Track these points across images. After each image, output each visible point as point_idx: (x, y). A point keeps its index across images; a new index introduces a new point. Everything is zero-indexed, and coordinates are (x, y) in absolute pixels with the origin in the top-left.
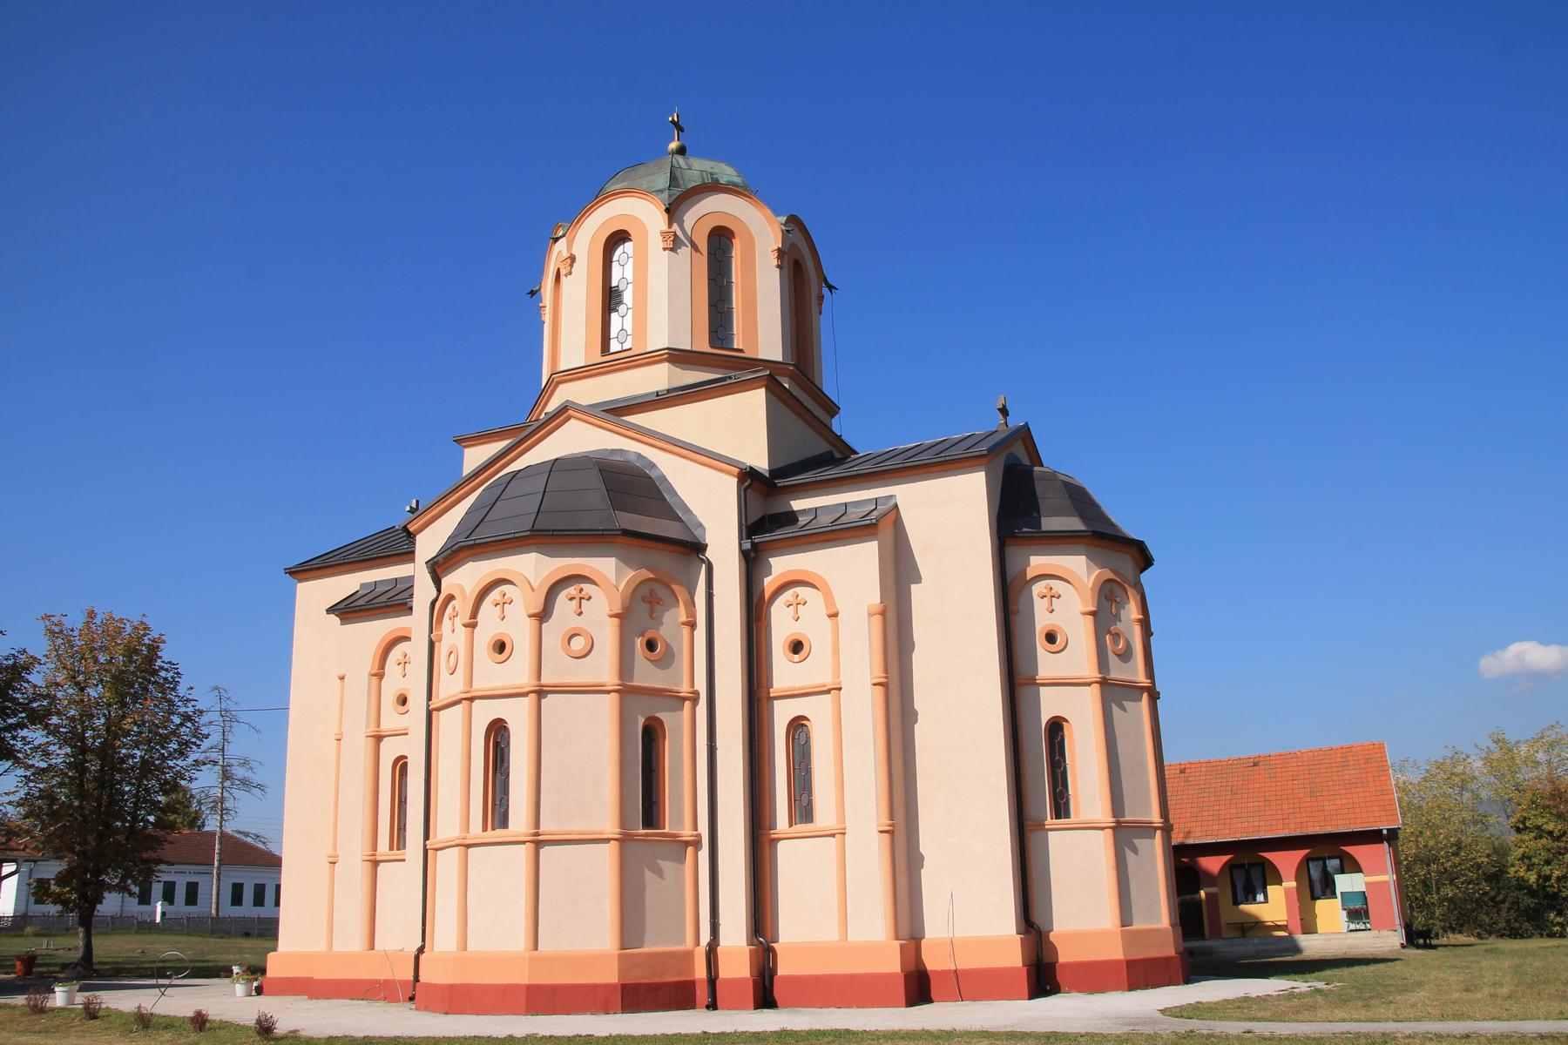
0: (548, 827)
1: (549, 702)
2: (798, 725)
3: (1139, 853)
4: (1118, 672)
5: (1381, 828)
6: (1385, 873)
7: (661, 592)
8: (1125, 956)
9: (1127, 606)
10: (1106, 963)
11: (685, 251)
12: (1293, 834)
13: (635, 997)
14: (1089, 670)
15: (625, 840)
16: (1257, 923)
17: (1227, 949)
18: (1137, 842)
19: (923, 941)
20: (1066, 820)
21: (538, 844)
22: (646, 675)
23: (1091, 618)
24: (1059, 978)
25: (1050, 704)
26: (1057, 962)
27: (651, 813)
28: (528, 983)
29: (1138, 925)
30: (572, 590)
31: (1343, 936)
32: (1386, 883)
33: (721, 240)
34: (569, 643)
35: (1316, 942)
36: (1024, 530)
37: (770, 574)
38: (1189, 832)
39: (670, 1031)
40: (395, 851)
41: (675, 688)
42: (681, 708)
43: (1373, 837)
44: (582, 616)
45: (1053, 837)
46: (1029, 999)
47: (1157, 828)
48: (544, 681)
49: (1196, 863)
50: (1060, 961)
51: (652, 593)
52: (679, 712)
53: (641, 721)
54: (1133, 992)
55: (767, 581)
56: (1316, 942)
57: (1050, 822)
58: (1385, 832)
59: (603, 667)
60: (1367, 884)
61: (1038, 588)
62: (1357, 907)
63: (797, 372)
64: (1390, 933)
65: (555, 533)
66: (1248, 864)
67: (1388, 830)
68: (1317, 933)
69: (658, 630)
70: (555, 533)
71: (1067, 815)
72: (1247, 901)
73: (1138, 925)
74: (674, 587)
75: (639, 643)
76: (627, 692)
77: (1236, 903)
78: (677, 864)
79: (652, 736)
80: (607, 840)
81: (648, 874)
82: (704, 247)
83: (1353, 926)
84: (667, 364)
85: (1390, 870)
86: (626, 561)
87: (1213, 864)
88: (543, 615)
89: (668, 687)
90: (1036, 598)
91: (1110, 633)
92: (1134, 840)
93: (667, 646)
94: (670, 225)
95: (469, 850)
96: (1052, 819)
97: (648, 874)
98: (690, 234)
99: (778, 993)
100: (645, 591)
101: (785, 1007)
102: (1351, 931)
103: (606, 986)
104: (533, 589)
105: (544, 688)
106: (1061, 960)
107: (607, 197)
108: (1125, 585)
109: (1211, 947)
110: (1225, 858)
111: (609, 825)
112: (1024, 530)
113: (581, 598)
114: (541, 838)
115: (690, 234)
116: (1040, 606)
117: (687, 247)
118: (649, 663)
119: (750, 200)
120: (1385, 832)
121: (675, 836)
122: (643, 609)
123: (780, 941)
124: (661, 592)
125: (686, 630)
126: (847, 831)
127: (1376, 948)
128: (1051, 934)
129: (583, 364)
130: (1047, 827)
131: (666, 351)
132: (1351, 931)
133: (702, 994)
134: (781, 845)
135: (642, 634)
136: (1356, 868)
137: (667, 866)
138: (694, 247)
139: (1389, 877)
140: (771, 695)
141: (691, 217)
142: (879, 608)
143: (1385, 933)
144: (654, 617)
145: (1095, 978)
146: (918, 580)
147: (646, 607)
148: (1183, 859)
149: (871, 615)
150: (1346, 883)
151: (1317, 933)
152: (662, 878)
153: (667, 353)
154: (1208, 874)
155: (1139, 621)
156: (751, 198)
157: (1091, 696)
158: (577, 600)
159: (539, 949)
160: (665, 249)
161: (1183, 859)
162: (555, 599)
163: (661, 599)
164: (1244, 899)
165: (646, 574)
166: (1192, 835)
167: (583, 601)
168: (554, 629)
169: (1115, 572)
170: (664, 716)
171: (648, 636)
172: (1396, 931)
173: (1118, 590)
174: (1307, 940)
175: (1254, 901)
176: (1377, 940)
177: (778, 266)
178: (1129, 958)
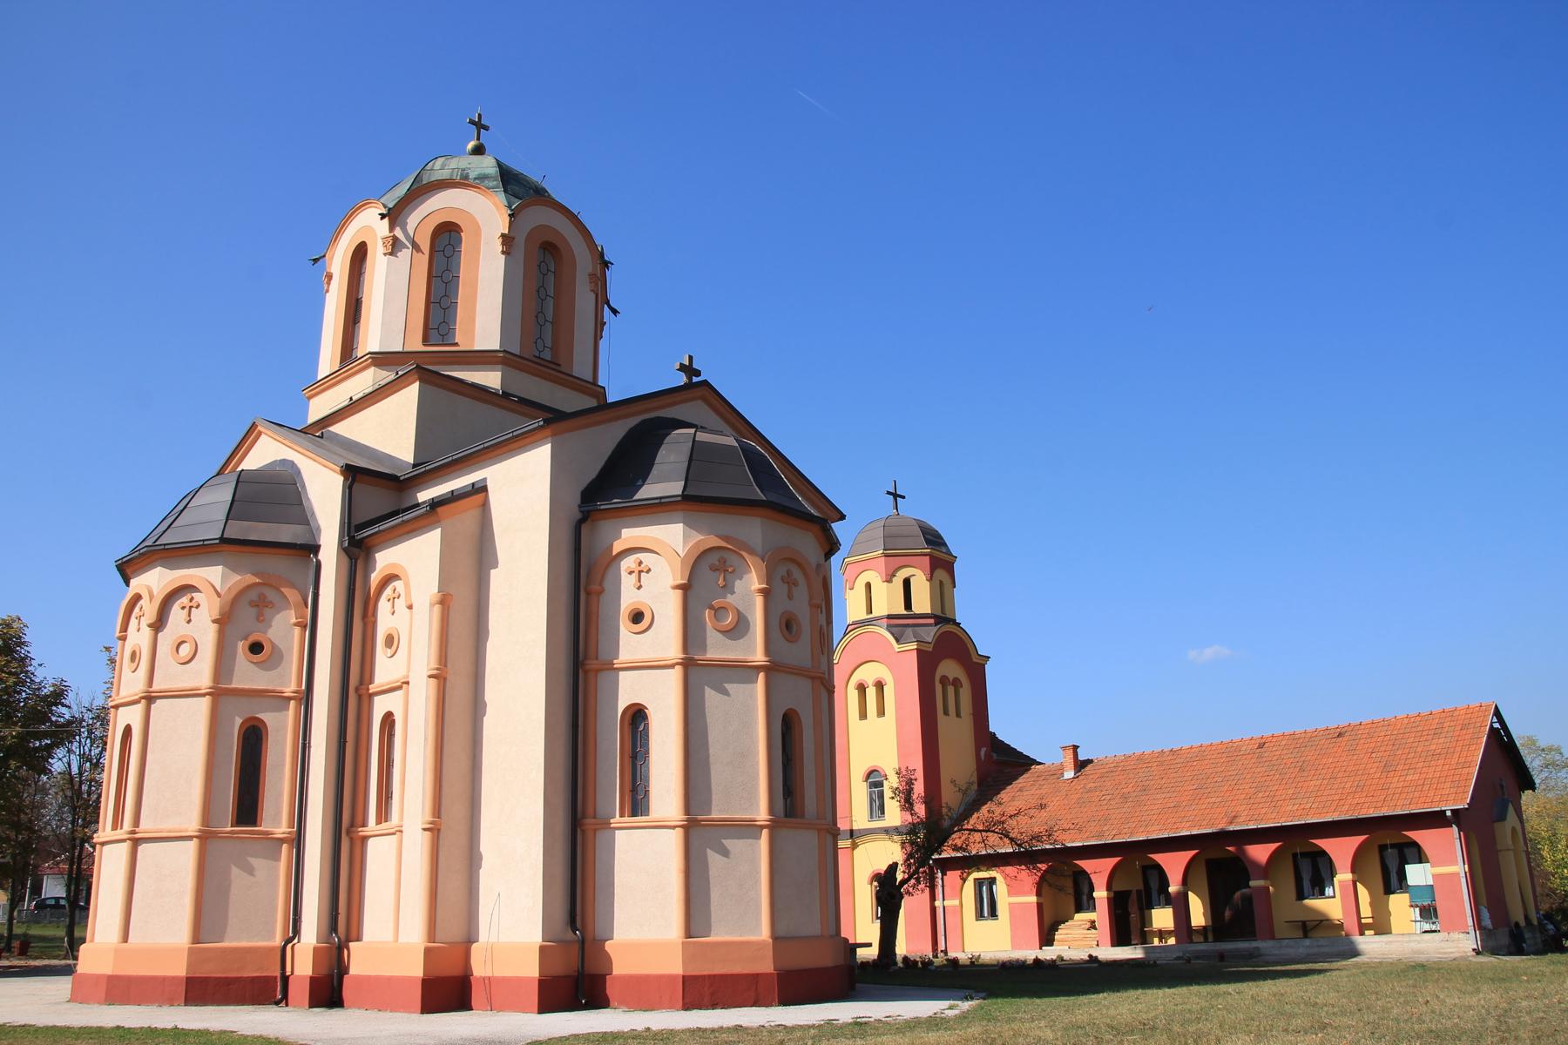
0: (147, 825)
1: (158, 706)
2: (388, 719)
3: (731, 856)
4: (718, 649)
5: (1443, 809)
6: (1453, 862)
7: (271, 595)
8: (684, 971)
9: (746, 577)
10: (660, 978)
11: (405, 254)
12: (1343, 817)
13: (200, 990)
14: (674, 651)
15: (206, 837)
16: (1322, 921)
17: (1277, 952)
18: (727, 843)
19: (474, 945)
20: (644, 818)
21: (136, 842)
22: (247, 675)
23: (679, 592)
24: (609, 991)
25: (630, 690)
26: (472, 975)
27: (248, 808)
28: (110, 973)
29: (718, 935)
30: (184, 600)
31: (1418, 938)
32: (1457, 874)
33: (447, 236)
34: (178, 652)
35: (1375, 945)
36: (615, 501)
37: (375, 570)
38: (1235, 817)
39: (718, 1012)
40: (626, 819)
41: (278, 689)
42: (287, 709)
43: (1435, 820)
44: (191, 624)
45: (621, 837)
46: (422, 1013)
47: (762, 827)
48: (156, 687)
49: (1244, 852)
50: (614, 973)
51: (262, 597)
52: (285, 712)
53: (238, 721)
54: (688, 1012)
55: (373, 576)
56: (1375, 945)
57: (616, 820)
58: (1449, 813)
59: (201, 674)
60: (1435, 876)
61: (628, 563)
62: (1425, 903)
63: (507, 355)
64: (1462, 936)
65: (166, 547)
66: (1301, 853)
67: (1451, 810)
68: (1391, 933)
69: (265, 633)
70: (166, 547)
71: (646, 812)
72: (1313, 896)
73: (718, 935)
74: (282, 589)
75: (242, 647)
76: (220, 694)
77: (1301, 896)
78: (270, 862)
79: (253, 740)
80: (189, 838)
81: (235, 871)
82: (425, 245)
83: (1427, 927)
84: (373, 368)
85: (1460, 858)
86: (234, 568)
87: (1260, 853)
88: (159, 624)
89: (270, 688)
90: (624, 574)
91: (711, 607)
92: (723, 841)
93: (273, 645)
94: (392, 229)
95: (104, 847)
96: (622, 815)
97: (235, 871)
98: (412, 235)
99: (347, 993)
100: (253, 595)
101: (355, 1007)
102: (1426, 932)
103: (174, 978)
104: (219, 595)
105: (153, 694)
106: (618, 970)
107: (355, 211)
108: (744, 553)
109: (1257, 948)
110: (1273, 846)
111: (191, 822)
112: (615, 501)
113: (191, 607)
114: (137, 836)
115: (412, 235)
116: (627, 582)
117: (408, 248)
118: (252, 665)
119: (484, 193)
120: (1449, 813)
121: (267, 833)
122: (247, 613)
123: (364, 940)
124: (271, 595)
125: (297, 630)
126: (403, 829)
127: (1445, 953)
128: (607, 943)
129: (328, 374)
130: (612, 826)
131: (369, 356)
132: (1426, 932)
133: (300, 991)
134: (371, 842)
135: (246, 638)
136: (1420, 858)
137: (257, 863)
138: (416, 247)
139: (1459, 868)
140: (370, 691)
141: (413, 220)
142: (437, 597)
143: (1456, 935)
144: (262, 620)
145: (646, 993)
146: (741, 580)
147: (253, 611)
148: (1229, 848)
149: (432, 605)
150: (1416, 874)
151: (1391, 933)
152: (252, 875)
153: (370, 358)
154: (1255, 864)
155: (761, 591)
156: (479, 188)
157: (672, 680)
158: (186, 610)
159: (129, 941)
160: (385, 254)
161: (1229, 848)
162: (171, 609)
163: (271, 602)
164: (1311, 893)
165: (251, 579)
166: (1237, 820)
167: (193, 609)
168: (167, 638)
169: (726, 539)
170: (268, 718)
171: (252, 639)
172: (1468, 933)
173: (732, 559)
174: (1366, 943)
175: (1322, 893)
176: (1443, 944)
177: (503, 252)
178: (688, 974)
